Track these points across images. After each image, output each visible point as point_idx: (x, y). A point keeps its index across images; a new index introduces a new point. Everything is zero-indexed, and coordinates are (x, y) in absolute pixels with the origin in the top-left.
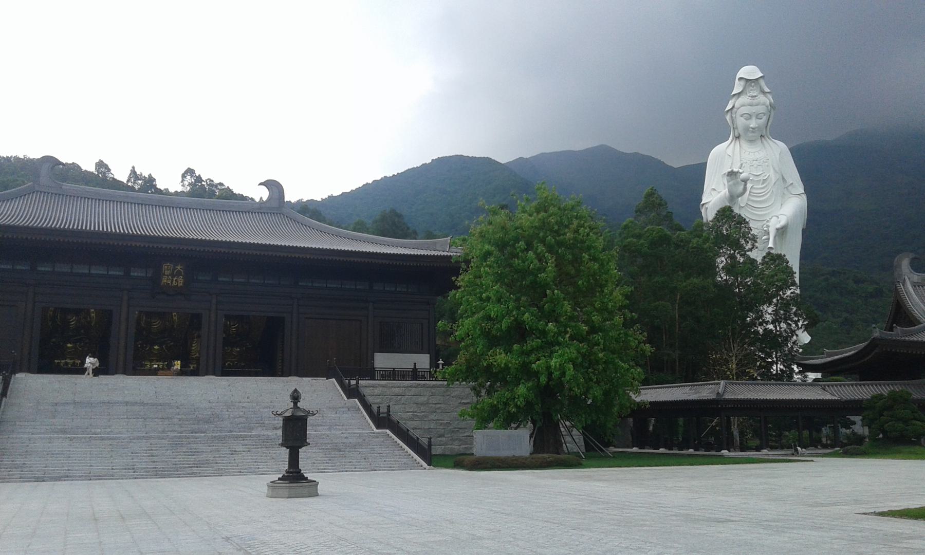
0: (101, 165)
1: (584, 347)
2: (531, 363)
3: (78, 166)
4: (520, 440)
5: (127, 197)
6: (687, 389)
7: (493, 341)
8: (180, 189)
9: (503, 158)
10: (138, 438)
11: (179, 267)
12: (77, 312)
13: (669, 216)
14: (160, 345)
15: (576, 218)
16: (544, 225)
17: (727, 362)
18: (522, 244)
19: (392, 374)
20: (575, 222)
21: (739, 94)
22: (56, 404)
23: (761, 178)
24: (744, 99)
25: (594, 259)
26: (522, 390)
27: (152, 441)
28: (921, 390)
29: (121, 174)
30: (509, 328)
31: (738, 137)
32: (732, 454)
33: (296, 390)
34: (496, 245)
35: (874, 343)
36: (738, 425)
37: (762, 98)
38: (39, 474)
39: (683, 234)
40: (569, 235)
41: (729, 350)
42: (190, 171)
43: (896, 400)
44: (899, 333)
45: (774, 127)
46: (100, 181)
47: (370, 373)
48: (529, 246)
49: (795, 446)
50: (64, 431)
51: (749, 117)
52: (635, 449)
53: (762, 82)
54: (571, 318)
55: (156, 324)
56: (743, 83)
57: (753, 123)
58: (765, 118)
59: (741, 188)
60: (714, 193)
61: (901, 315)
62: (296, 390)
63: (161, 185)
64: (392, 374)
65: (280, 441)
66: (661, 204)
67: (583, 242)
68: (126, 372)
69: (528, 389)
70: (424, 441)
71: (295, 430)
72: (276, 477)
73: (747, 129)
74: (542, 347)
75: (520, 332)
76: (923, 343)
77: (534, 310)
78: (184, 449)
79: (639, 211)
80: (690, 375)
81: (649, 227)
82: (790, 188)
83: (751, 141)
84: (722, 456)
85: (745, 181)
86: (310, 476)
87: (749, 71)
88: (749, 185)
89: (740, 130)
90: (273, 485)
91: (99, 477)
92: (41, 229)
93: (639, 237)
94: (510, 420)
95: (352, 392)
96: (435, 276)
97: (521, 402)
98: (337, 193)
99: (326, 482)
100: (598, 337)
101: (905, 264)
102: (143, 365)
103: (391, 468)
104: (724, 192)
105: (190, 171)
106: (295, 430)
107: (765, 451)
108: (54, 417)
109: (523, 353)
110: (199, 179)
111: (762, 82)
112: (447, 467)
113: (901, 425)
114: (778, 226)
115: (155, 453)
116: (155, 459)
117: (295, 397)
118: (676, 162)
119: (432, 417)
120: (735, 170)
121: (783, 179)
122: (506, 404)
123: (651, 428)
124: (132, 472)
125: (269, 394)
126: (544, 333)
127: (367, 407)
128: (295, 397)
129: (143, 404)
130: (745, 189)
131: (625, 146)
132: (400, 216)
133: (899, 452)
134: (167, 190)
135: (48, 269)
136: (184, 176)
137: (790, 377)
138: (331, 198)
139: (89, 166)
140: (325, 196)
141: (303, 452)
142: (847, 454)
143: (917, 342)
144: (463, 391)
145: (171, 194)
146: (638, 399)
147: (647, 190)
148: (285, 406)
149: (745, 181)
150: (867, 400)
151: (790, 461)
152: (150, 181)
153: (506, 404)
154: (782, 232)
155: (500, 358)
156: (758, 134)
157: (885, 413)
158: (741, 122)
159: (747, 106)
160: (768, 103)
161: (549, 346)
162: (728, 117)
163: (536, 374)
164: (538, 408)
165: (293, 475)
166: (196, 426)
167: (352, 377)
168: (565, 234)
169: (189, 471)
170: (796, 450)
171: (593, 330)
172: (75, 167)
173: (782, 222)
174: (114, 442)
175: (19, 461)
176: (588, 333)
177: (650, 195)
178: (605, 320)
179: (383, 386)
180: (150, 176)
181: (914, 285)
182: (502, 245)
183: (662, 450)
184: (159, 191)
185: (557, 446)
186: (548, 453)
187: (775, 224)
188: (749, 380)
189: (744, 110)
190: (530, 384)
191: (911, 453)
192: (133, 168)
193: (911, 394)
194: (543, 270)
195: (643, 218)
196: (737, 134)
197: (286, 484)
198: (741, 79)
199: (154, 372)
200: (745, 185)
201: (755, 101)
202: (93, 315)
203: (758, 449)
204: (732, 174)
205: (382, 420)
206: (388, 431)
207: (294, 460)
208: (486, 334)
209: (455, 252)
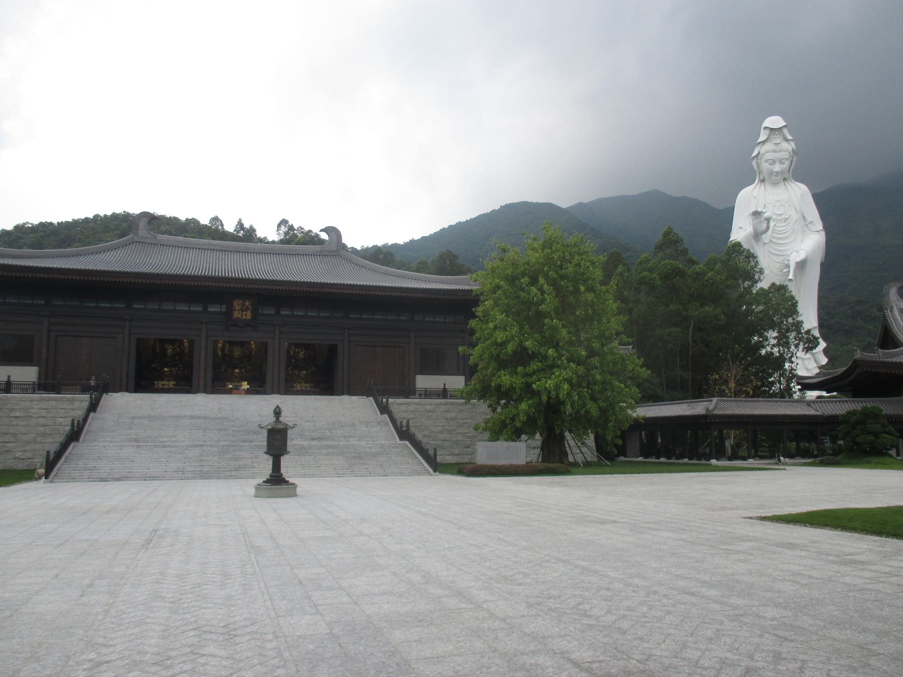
0: (216, 219)
1: (581, 370)
2: (532, 383)
3: (198, 222)
4: (523, 450)
5: (210, 245)
6: (685, 405)
7: (503, 364)
8: (276, 238)
9: (564, 203)
10: (195, 446)
11: (247, 303)
12: (172, 342)
13: (684, 252)
14: (240, 368)
15: (579, 254)
16: (549, 261)
17: (726, 382)
18: (525, 280)
19: (428, 394)
20: (577, 257)
21: (764, 142)
22: (134, 418)
23: (783, 216)
24: (769, 146)
25: (591, 289)
26: (523, 406)
27: (205, 449)
28: (888, 406)
29: (230, 227)
30: (515, 352)
31: (763, 181)
32: (720, 463)
33: (278, 407)
34: (506, 278)
35: (856, 364)
36: (735, 438)
37: (785, 145)
38: (105, 475)
39: (698, 268)
40: (571, 269)
41: (729, 370)
42: (284, 222)
43: (867, 416)
44: (880, 355)
45: (798, 172)
46: (213, 232)
47: (408, 391)
48: (534, 281)
49: (779, 456)
50: (136, 440)
51: (773, 162)
52: (641, 459)
53: (785, 131)
54: (571, 343)
55: (237, 352)
56: (767, 132)
57: (777, 168)
58: (787, 163)
59: (765, 225)
60: (741, 231)
61: (888, 339)
62: (278, 407)
63: (260, 234)
64: (428, 394)
65: (265, 450)
66: (677, 241)
67: (583, 274)
68: (206, 391)
69: (530, 406)
70: (431, 452)
71: (277, 441)
72: (261, 481)
73: (771, 173)
74: (543, 370)
75: (522, 357)
76: (900, 363)
77: (538, 336)
78: (229, 456)
79: (659, 247)
80: (699, 392)
81: (666, 261)
82: (810, 226)
83: (775, 184)
84: (710, 465)
85: (768, 220)
86: (291, 480)
87: (775, 121)
88: (772, 224)
89: (765, 174)
90: (258, 487)
91: (153, 478)
92: (158, 275)
93: (651, 270)
94: (516, 435)
95: (384, 409)
96: (461, 306)
97: (523, 417)
98: (417, 237)
99: (303, 485)
100: (595, 360)
101: (893, 293)
102: (225, 386)
103: (401, 474)
104: (749, 229)
105: (284, 222)
106: (277, 441)
107: (751, 461)
108: (130, 429)
109: (527, 375)
110: (291, 228)
111: (785, 131)
112: (453, 474)
113: (871, 438)
114: (798, 260)
115: (205, 458)
116: (203, 463)
117: (277, 413)
118: (720, 207)
119: (459, 430)
120: (759, 210)
121: (804, 218)
122: (513, 419)
123: (659, 441)
124: (182, 475)
125: (253, 409)
126: (545, 357)
127: (393, 421)
128: (277, 413)
129: (206, 418)
130: (768, 228)
131: (675, 191)
132: (455, 257)
133: (869, 463)
134: (265, 238)
135: (142, 306)
136: (279, 226)
137: (791, 395)
138: (412, 242)
139: (205, 221)
140: (407, 240)
141: (284, 460)
142: (823, 464)
143: (896, 363)
144: (481, 410)
145: (268, 243)
146: (635, 415)
147: (665, 229)
148: (269, 419)
149: (768, 220)
150: (843, 415)
151: (772, 469)
152: (252, 230)
153: (513, 419)
154: (802, 265)
155: (505, 379)
156: (780, 178)
157: (858, 427)
158: (765, 166)
159: (775, 152)
160: (790, 149)
161: (550, 368)
162: (754, 163)
163: (537, 393)
164: (540, 422)
165: (277, 480)
166: (247, 437)
167: (383, 395)
168: (567, 268)
169: (228, 473)
170: (779, 460)
171: (592, 353)
172: (194, 222)
173: (802, 256)
174: (173, 449)
175: (91, 464)
176: (588, 357)
177: (666, 234)
178: (603, 345)
179: (416, 404)
180: (251, 227)
182: (512, 280)
183: (662, 460)
184: (261, 240)
185: (562, 455)
186: (553, 461)
187: (796, 257)
188: (746, 397)
189: (769, 156)
190: (530, 402)
191: (877, 463)
192: (240, 220)
193: (881, 410)
194: (543, 301)
195: (660, 255)
196: (762, 178)
197: (268, 486)
198: (765, 128)
199: (230, 392)
200: (768, 223)
201: (778, 149)
202: (253, 346)
203: (744, 459)
204: (756, 214)
205: (404, 433)
206: (407, 443)
207: (276, 466)
208: (497, 358)
209: (475, 287)
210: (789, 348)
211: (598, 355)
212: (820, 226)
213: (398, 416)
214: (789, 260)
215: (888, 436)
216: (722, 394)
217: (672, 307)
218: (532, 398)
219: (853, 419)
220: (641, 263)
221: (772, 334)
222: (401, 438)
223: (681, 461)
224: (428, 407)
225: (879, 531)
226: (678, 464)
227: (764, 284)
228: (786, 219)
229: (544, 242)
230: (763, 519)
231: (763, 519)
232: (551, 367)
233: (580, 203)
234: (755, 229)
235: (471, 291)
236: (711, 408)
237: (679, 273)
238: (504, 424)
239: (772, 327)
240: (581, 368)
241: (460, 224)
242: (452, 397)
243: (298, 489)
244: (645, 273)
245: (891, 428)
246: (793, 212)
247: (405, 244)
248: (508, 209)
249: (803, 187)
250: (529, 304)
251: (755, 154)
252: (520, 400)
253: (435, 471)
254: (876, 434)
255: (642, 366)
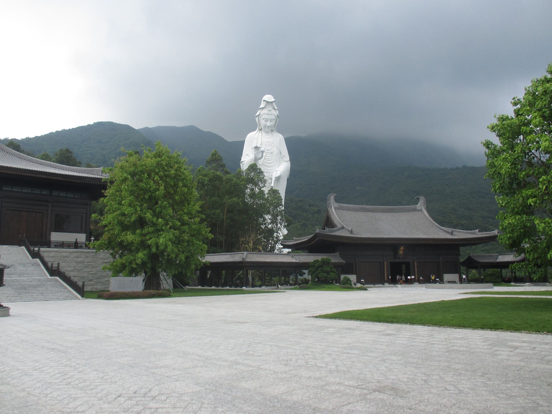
4: (137, 283)
7: (125, 228)
19: (62, 245)
21: (263, 108)
23: (270, 151)
31: (261, 130)
32: (248, 289)
34: (130, 174)
35: (316, 235)
40: (173, 172)
41: (249, 237)
43: (325, 263)
47: (48, 244)
52: (200, 287)
53: (274, 104)
56: (265, 103)
57: (268, 124)
58: (274, 122)
60: (247, 156)
64: (62, 245)
66: (220, 159)
73: (265, 126)
79: (209, 163)
85: (263, 152)
87: (269, 98)
88: (264, 154)
93: (205, 175)
94: (133, 272)
95: (35, 255)
100: (186, 227)
101: (332, 198)
103: (58, 299)
107: (263, 287)
111: (274, 104)
112: (93, 298)
113: (325, 275)
114: (276, 176)
118: (229, 138)
119: (85, 270)
120: (258, 146)
130: (262, 156)
133: (324, 288)
140: (24, 137)
144: (105, 256)
146: (204, 261)
147: (213, 151)
149: (263, 152)
153: (130, 263)
154: (278, 179)
155: (129, 237)
157: (319, 269)
158: (263, 122)
159: (267, 115)
161: (158, 231)
162: (257, 119)
163: (149, 246)
170: (278, 287)
177: (214, 155)
179: (56, 252)
181: (335, 208)
183: (213, 287)
186: (153, 289)
189: (264, 116)
191: (329, 288)
198: (264, 101)
201: (270, 113)
203: (260, 286)
204: (257, 148)
205: (54, 271)
206: (57, 278)
208: (121, 223)
210: (277, 225)
211: (187, 224)
212: (288, 158)
213: (47, 259)
214: (272, 176)
215: (333, 274)
216: (246, 250)
217: (214, 199)
218: (144, 250)
219: (317, 265)
220: (199, 171)
221: (268, 217)
222: (51, 275)
223: (225, 288)
224: (64, 254)
225: (412, 321)
226: (223, 290)
227: (421, 205)
228: (272, 153)
229: (156, 153)
230: (316, 317)
231: (316, 317)
232: (158, 231)
233: (147, 128)
234: (255, 157)
235: (102, 179)
236: (244, 257)
237: (219, 178)
238: (123, 267)
239: (269, 213)
240: (177, 231)
241: (64, 131)
242: (81, 247)
243: (10, 310)
244: (200, 176)
245: (334, 270)
246: (275, 149)
247: (22, 139)
248: (99, 125)
249: (281, 136)
250: (146, 191)
251: (258, 114)
252: (137, 251)
253: (83, 297)
254: (328, 273)
255: (210, 232)
